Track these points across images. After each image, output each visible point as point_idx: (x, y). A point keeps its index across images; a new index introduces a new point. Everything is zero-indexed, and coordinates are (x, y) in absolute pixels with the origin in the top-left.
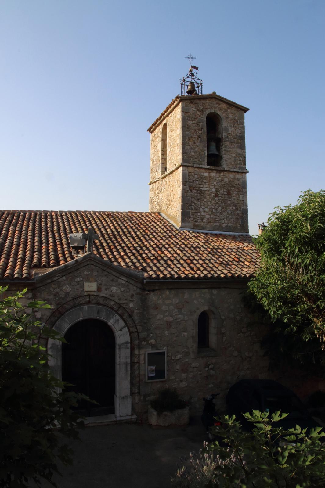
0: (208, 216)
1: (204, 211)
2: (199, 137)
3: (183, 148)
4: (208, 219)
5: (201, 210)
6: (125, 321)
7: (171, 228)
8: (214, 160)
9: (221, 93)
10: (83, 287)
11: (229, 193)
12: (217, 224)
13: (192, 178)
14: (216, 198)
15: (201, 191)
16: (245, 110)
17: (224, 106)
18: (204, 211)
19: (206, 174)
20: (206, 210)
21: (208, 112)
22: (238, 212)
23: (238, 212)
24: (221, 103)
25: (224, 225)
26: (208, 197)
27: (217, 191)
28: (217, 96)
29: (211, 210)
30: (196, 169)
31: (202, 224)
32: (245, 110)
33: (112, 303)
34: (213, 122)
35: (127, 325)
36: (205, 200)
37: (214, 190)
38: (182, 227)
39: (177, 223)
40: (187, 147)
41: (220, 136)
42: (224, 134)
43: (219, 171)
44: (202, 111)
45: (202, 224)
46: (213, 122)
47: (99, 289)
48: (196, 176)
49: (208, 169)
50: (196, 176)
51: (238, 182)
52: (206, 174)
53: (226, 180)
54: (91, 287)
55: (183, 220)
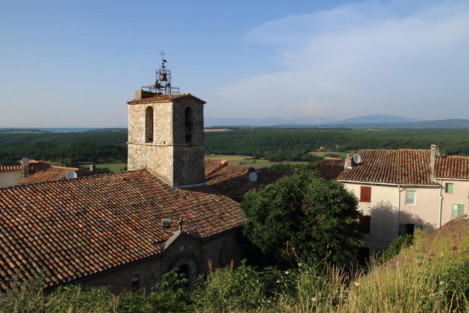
0: (186, 176)
1: (184, 173)
2: (181, 124)
3: (174, 134)
4: (186, 178)
5: (183, 173)
6: (195, 262)
7: (166, 186)
8: (188, 138)
9: (193, 94)
10: (179, 249)
11: (196, 160)
12: (190, 180)
13: (178, 153)
14: (190, 164)
15: (182, 160)
16: (205, 103)
17: (194, 101)
18: (184, 173)
19: (185, 149)
20: (185, 172)
21: (186, 106)
22: (200, 171)
23: (200, 171)
24: (192, 100)
25: (194, 180)
26: (186, 164)
27: (190, 159)
28: (192, 96)
29: (187, 172)
30: (180, 147)
31: (183, 181)
32: (205, 103)
33: (190, 254)
34: (188, 111)
35: (195, 264)
36: (184, 166)
37: (189, 159)
38: (174, 185)
39: (171, 184)
40: (176, 132)
41: (191, 122)
42: (194, 121)
43: (191, 146)
44: (183, 107)
45: (183, 181)
46: (188, 111)
47: (185, 249)
48: (180, 151)
49: (186, 146)
50: (180, 151)
51: (200, 151)
52: (185, 149)
53: (194, 150)
54: (182, 249)
55: (174, 181)
